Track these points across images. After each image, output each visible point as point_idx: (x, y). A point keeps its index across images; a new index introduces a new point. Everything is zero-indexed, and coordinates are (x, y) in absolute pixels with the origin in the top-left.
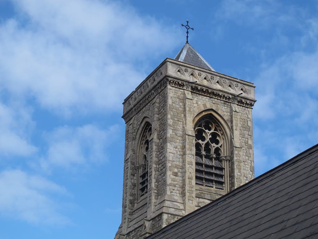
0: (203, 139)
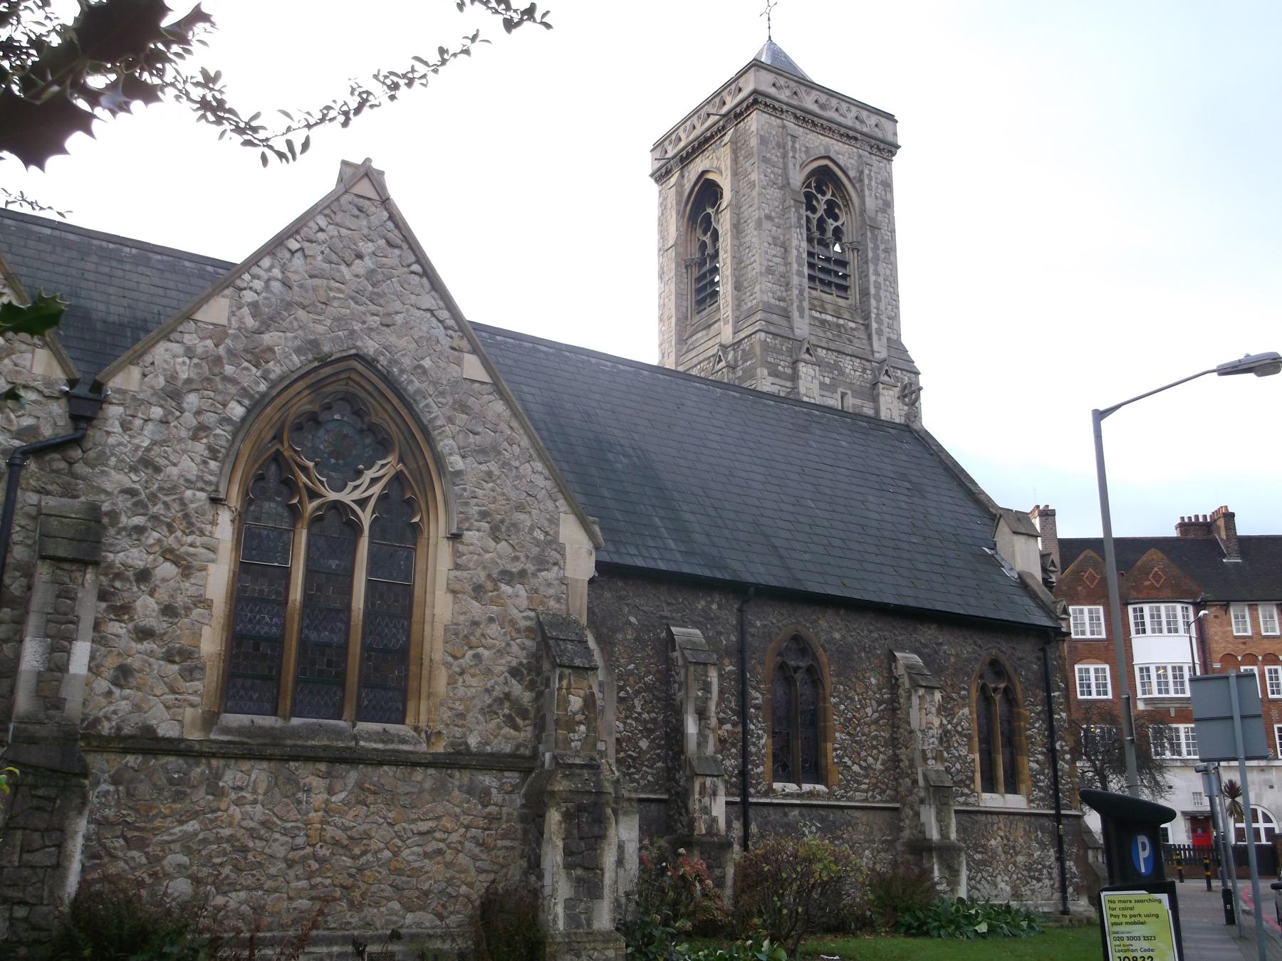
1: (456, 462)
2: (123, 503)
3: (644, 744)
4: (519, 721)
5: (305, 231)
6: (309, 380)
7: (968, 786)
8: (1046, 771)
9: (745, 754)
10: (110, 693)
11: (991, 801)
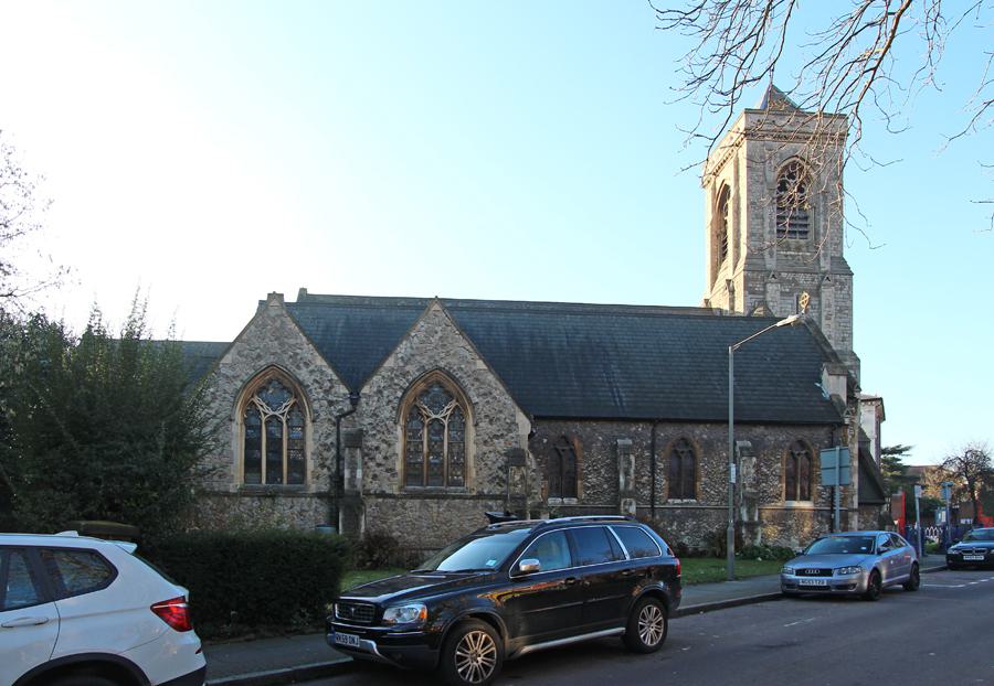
1: (475, 400)
3: (605, 486)
9: (653, 489)
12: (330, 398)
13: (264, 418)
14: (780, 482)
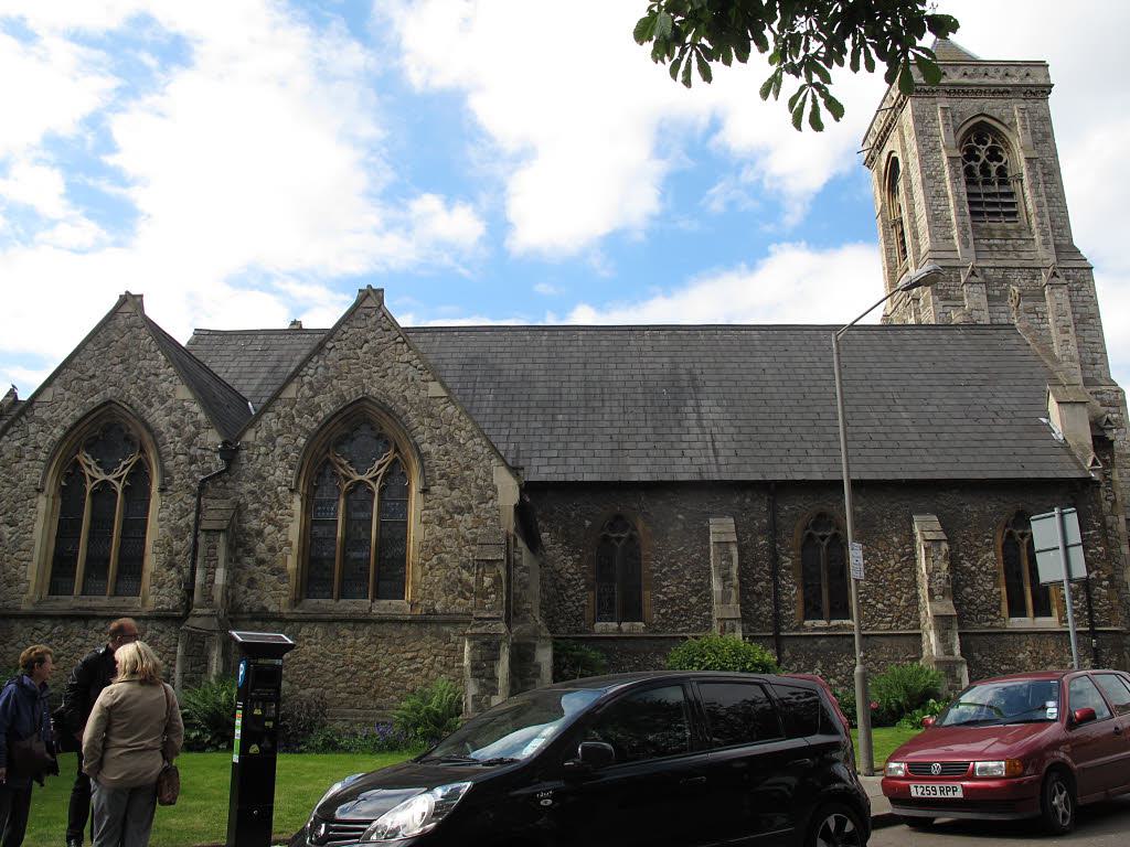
0: (977, 159)
1: (425, 447)
2: (249, 498)
4: (468, 594)
5: (336, 336)
6: (340, 416)
7: (994, 613)
8: (1081, 596)
10: (245, 592)
11: (1017, 623)
12: (192, 450)
13: (89, 487)
14: (996, 585)
